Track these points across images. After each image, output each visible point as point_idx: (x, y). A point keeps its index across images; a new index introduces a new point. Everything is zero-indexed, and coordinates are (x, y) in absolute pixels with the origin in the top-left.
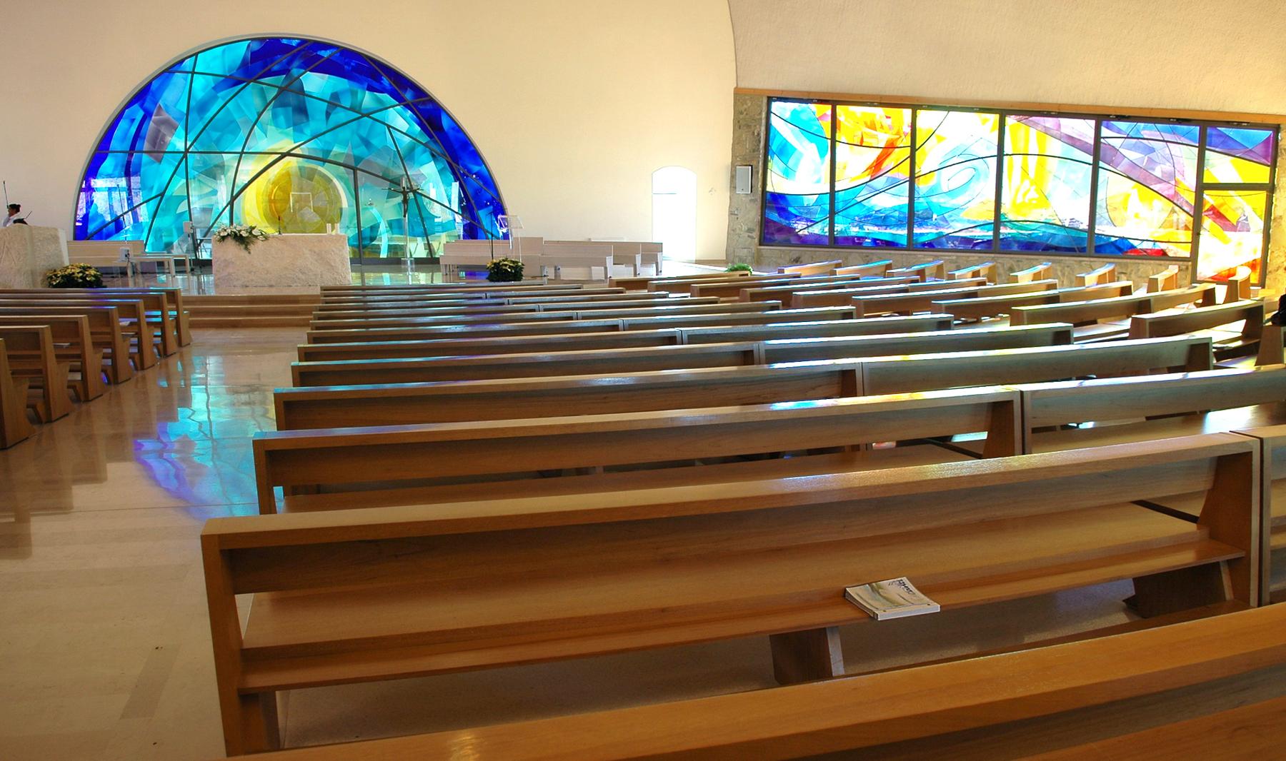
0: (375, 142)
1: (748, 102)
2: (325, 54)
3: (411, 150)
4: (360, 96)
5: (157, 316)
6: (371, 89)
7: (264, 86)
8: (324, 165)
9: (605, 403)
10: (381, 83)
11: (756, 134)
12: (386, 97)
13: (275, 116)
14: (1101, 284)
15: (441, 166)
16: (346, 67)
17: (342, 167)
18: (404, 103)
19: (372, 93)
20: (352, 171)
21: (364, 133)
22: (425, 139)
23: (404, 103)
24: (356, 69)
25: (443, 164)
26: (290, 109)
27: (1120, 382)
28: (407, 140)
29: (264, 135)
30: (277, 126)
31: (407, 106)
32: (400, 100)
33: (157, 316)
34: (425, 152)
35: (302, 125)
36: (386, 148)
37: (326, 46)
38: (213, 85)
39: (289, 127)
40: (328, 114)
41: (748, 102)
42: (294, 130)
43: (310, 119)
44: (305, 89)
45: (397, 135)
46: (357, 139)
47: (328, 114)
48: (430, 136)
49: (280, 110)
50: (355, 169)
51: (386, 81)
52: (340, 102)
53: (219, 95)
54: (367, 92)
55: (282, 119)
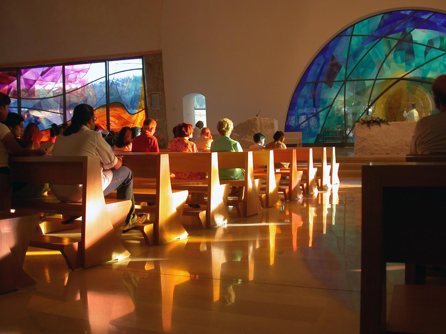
16: (438, 24)
26: (404, 51)
30: (396, 62)
38: (362, 41)
42: (406, 64)
49: (398, 53)
53: (365, 47)
55: (399, 58)
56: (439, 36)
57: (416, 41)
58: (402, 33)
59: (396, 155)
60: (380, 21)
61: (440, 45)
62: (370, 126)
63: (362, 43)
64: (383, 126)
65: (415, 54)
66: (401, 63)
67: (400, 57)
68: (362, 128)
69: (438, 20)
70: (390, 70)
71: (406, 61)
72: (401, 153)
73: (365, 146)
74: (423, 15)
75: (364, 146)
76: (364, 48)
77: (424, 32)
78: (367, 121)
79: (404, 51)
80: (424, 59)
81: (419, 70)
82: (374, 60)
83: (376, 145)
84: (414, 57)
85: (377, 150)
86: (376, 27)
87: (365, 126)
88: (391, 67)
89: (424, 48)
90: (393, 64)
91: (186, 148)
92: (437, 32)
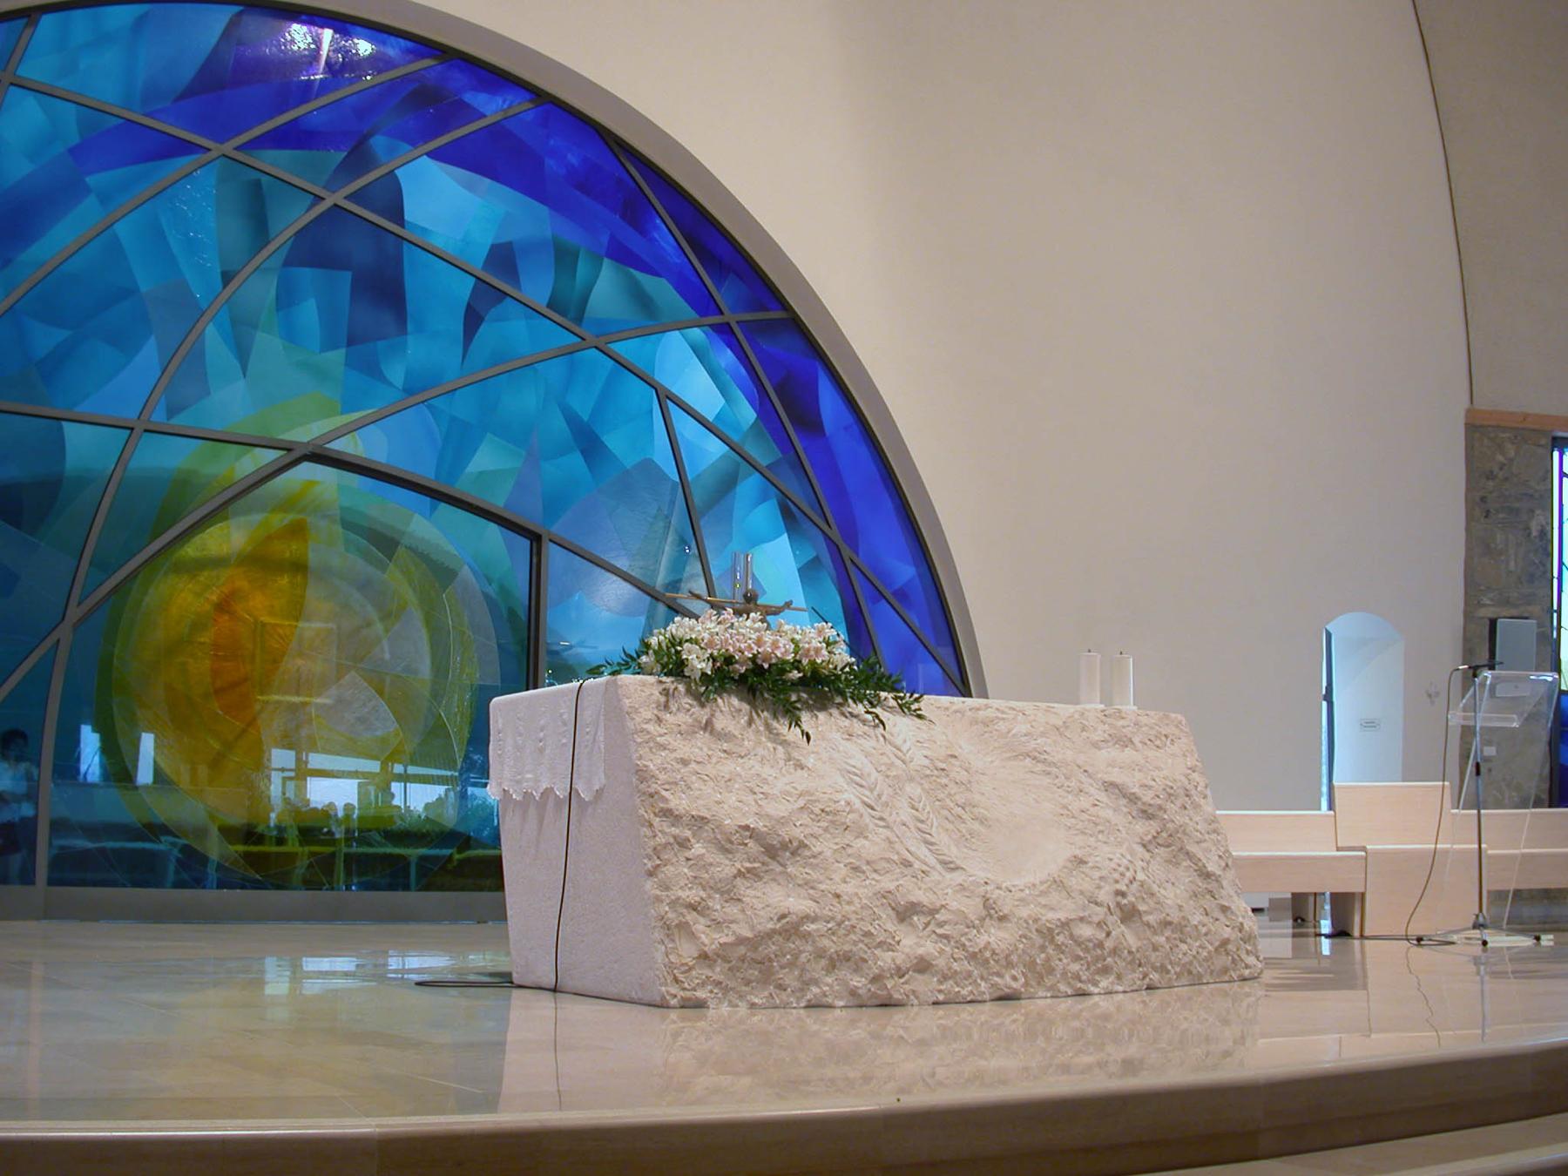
0: (614, 442)
1: (1509, 446)
2: (492, 108)
3: (726, 484)
4: (582, 269)
5: (473, 778)
6: (622, 255)
7: (265, 179)
8: (433, 509)
9: (1098, 801)
10: (652, 240)
11: (1535, 533)
12: (661, 290)
13: (286, 299)
14: (358, 204)
15: (810, 554)
16: (550, 163)
17: (493, 529)
18: (716, 319)
19: (622, 266)
20: (524, 544)
21: (583, 407)
22: (764, 453)
23: (716, 319)
24: (587, 182)
25: (815, 548)
26: (347, 276)
27: (466, 127)
28: (715, 449)
29: (236, 363)
30: (291, 335)
31: (724, 332)
32: (703, 304)
33: (473, 778)
34: (764, 498)
35: (381, 345)
36: (648, 467)
37: (495, 78)
38: (74, 138)
39: (335, 347)
40: (472, 320)
41: (1509, 446)
42: (349, 364)
43: (410, 327)
44: (406, 218)
45: (686, 428)
46: (559, 424)
47: (472, 320)
48: (785, 444)
49: (307, 276)
50: (535, 539)
51: (666, 237)
52: (515, 280)
53: (91, 180)
54: (607, 262)
55: (309, 312)
56: (549, 234)
57: (424, 230)
58: (346, 157)
59: (1070, 1001)
60: (214, 40)
61: (553, 289)
62: (826, 702)
63: (74, 152)
64: (824, 725)
65: (410, 307)
66: (322, 351)
67: (315, 306)
68: (708, 726)
69: (552, 142)
70: (241, 384)
71: (351, 342)
72: (1096, 984)
73: (807, 918)
74: (475, 89)
75: (791, 928)
76: (87, 190)
77: (470, 187)
78: (754, 659)
79: (347, 276)
80: (460, 350)
81: (427, 411)
82: (144, 287)
83: (906, 913)
84: (403, 330)
85: (923, 966)
86: (187, 72)
87: (730, 710)
88: (249, 367)
89: (463, 288)
90: (267, 343)
91: (836, 971)
92: (543, 210)
